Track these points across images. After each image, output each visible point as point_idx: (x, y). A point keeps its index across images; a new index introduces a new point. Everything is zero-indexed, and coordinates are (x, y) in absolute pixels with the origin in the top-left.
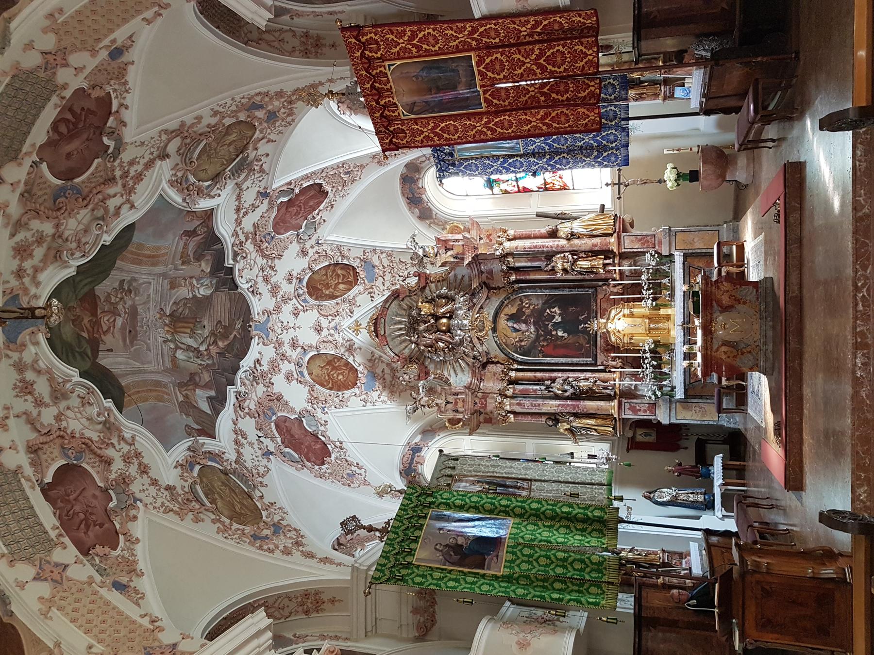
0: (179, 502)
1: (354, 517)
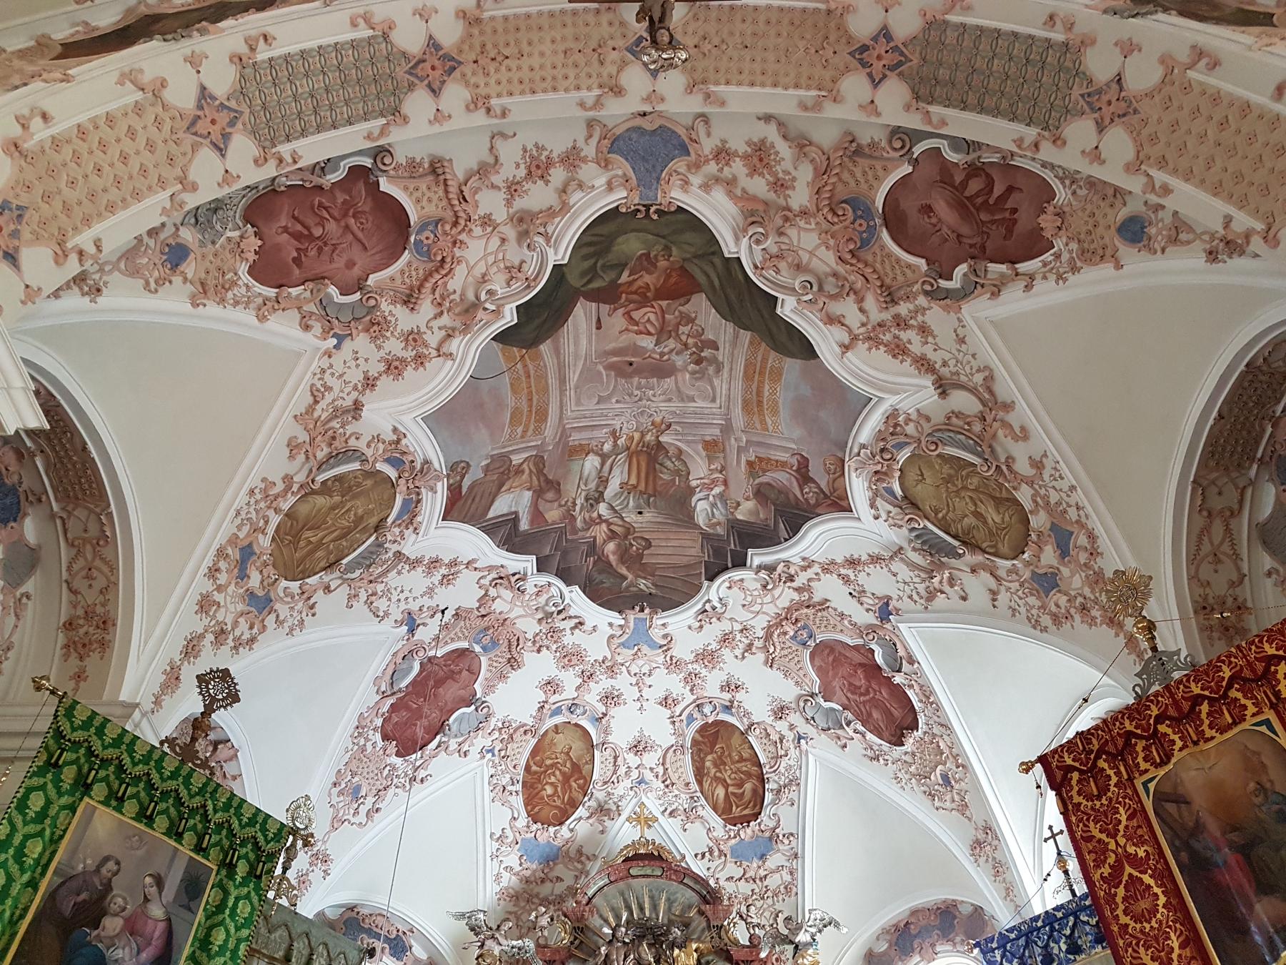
0: (330, 420)
1: (236, 699)
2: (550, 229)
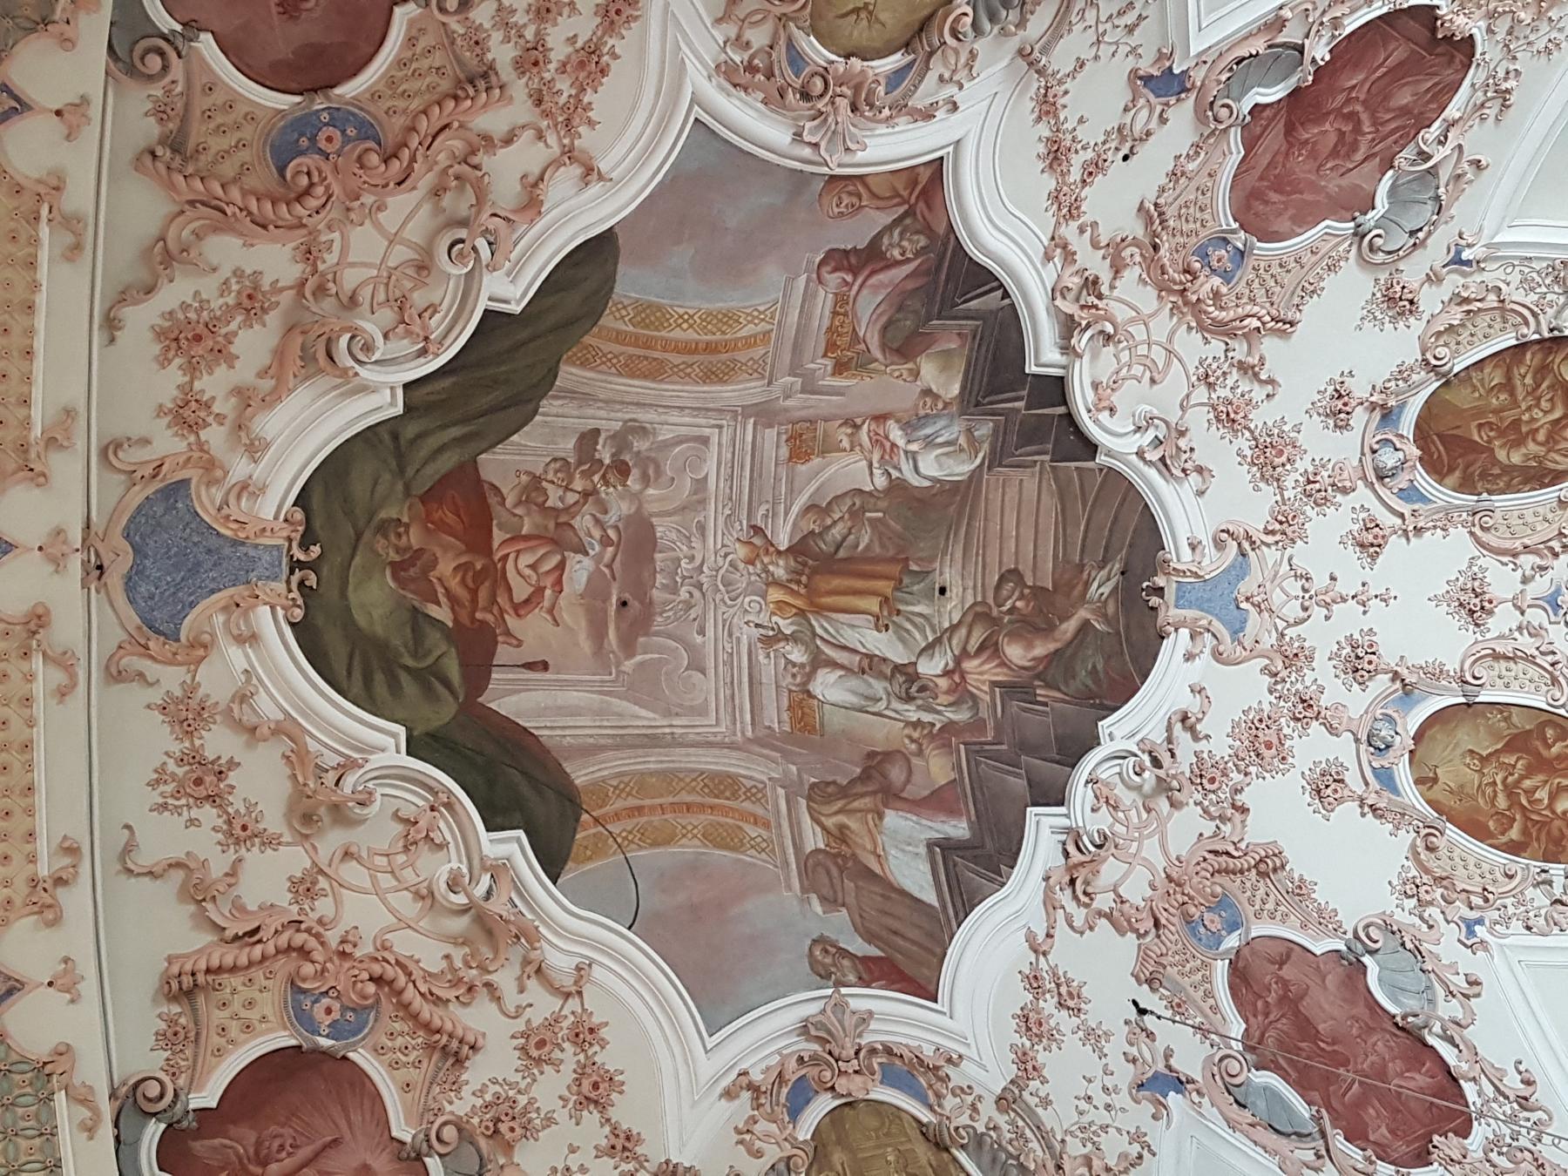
2: (331, 760)
